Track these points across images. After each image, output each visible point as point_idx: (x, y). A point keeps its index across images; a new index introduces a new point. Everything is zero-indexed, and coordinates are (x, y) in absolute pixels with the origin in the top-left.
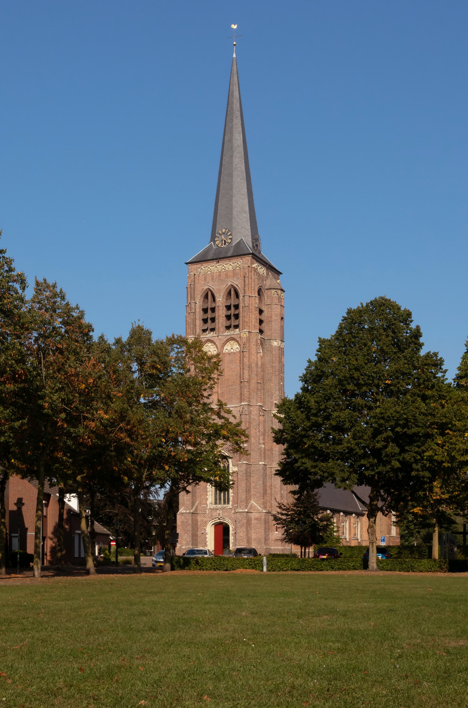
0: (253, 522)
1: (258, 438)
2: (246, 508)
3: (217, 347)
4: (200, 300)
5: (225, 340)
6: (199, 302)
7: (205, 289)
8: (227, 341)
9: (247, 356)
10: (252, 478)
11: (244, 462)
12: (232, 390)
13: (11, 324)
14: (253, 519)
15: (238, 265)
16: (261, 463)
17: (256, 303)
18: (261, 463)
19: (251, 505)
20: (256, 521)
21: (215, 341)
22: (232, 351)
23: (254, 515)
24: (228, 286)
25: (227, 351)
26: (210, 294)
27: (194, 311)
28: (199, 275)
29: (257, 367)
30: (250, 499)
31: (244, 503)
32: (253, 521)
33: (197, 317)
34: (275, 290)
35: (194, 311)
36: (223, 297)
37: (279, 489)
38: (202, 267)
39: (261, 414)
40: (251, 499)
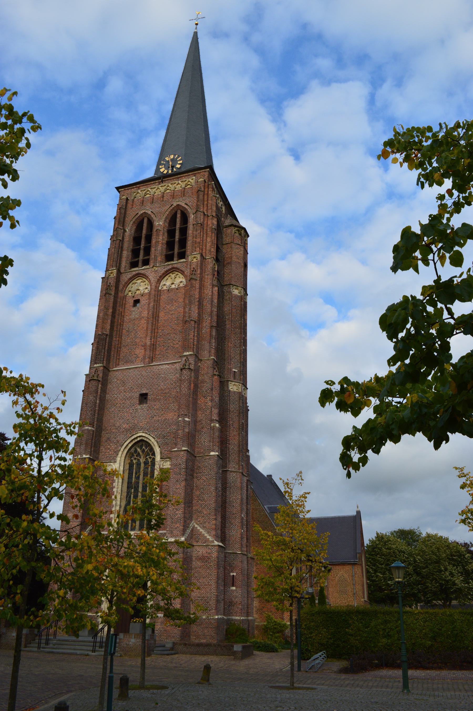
0: (196, 564)
1: (208, 411)
2: (183, 535)
3: (150, 281)
4: (132, 227)
5: (163, 272)
6: (130, 230)
7: (140, 213)
8: (166, 273)
9: (197, 286)
10: (195, 480)
11: (184, 449)
12: (169, 341)
13: (293, 685)
14: (194, 559)
15: (189, 183)
16: (212, 453)
17: (213, 224)
18: (212, 453)
19: (192, 530)
20: (199, 564)
21: (147, 274)
22: (173, 286)
23: (199, 551)
24: (173, 206)
25: (165, 288)
26: (146, 220)
27: (121, 238)
28: (133, 200)
29: (212, 304)
30: (191, 519)
31: (178, 525)
32: (194, 563)
33: (126, 245)
34: (236, 229)
35: (121, 238)
36: (165, 220)
37: (239, 508)
38: (139, 191)
39: (215, 373)
40: (191, 520)
